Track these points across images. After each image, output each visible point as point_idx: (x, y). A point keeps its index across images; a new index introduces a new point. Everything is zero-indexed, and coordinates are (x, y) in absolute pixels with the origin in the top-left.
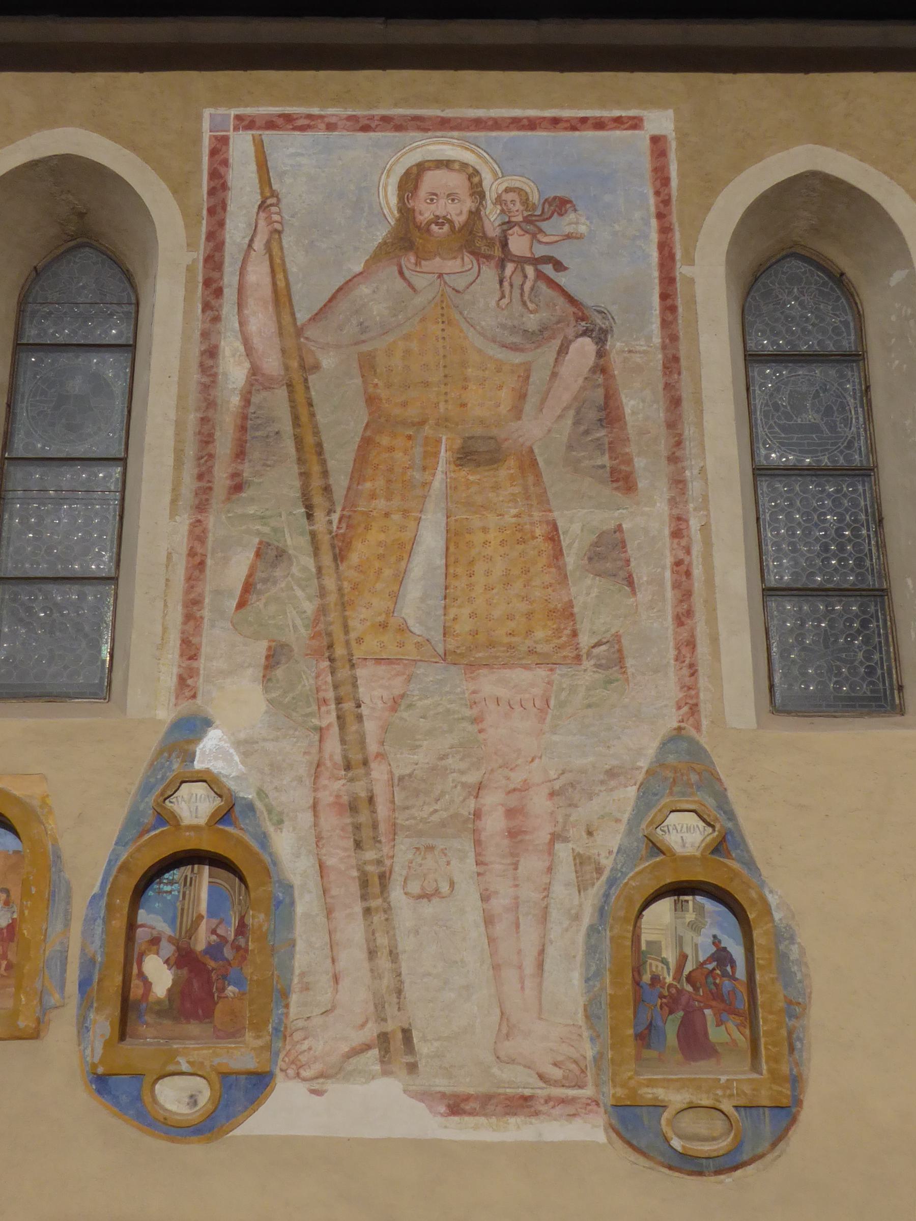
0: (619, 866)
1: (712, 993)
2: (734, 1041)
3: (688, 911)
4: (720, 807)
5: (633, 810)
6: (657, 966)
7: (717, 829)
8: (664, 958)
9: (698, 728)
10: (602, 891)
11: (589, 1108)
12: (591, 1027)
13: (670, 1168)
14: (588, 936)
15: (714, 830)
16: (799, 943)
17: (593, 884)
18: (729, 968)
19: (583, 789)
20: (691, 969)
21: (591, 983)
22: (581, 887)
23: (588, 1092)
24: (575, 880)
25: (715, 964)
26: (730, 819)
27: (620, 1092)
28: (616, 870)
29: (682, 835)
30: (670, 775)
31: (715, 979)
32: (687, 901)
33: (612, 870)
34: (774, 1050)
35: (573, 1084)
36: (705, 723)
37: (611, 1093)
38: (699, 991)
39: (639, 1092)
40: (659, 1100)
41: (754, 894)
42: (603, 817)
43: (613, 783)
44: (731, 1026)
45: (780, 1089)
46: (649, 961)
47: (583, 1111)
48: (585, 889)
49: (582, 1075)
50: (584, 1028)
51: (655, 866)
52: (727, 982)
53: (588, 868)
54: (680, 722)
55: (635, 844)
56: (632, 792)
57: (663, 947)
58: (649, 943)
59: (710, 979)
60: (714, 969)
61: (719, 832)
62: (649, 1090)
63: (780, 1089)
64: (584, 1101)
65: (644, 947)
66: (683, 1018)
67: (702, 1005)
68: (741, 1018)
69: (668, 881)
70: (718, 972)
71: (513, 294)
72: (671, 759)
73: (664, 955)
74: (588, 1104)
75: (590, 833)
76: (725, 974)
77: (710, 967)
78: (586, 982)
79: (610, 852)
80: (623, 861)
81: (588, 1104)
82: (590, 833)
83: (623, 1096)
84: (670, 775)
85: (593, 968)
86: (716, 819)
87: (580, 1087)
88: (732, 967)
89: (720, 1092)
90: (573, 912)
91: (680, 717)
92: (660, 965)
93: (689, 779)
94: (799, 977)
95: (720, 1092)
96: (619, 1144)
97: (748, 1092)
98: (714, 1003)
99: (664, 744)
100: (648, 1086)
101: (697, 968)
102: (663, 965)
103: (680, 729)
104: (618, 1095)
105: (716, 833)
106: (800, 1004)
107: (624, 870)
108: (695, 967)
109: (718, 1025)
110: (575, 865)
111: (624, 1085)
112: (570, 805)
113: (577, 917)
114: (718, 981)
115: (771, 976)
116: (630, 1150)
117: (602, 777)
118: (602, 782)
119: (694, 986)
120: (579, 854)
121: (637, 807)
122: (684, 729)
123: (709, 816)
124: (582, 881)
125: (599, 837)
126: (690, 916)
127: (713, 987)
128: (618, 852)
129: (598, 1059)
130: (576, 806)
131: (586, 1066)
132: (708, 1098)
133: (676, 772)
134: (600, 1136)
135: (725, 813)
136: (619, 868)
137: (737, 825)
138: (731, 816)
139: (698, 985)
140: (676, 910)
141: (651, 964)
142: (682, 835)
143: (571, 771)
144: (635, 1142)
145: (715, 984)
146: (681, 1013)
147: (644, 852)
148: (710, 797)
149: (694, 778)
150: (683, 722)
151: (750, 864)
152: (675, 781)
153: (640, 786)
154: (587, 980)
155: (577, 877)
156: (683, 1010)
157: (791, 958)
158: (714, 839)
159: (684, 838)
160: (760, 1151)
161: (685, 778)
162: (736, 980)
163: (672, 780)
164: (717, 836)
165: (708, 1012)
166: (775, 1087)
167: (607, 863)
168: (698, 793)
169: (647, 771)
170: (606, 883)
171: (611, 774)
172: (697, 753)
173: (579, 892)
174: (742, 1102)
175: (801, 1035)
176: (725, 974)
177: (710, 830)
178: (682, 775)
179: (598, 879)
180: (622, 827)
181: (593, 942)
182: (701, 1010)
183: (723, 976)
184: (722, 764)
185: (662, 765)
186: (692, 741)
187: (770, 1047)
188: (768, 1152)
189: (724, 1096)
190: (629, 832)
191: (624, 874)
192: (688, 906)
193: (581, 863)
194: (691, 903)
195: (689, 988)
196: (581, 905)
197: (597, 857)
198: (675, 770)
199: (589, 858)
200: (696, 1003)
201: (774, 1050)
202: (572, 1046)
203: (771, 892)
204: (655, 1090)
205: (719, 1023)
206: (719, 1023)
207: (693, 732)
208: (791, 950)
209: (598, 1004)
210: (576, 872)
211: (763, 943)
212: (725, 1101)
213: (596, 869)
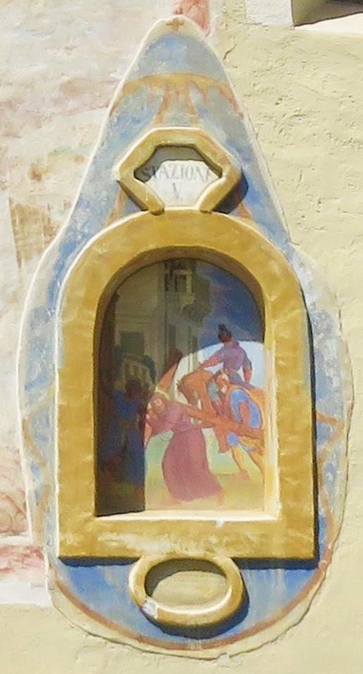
0: (79, 226)
1: (215, 407)
2: (243, 473)
3: (185, 290)
4: (231, 142)
5: (103, 144)
6: (136, 369)
7: (224, 174)
8: (147, 356)
9: (203, 23)
10: (52, 262)
11: (28, 560)
12: (34, 451)
13: (140, 639)
14: (32, 325)
15: (220, 176)
16: (339, 338)
17: (40, 251)
18: (241, 372)
19: (27, 111)
20: (186, 373)
21: (33, 390)
22: (22, 254)
23: (28, 538)
24: (14, 244)
25: (220, 366)
26: (247, 160)
27: (72, 539)
28: (75, 230)
29: (174, 181)
30: (159, 92)
31: (220, 386)
32: (184, 277)
33: (69, 229)
34: (295, 483)
35: (5, 528)
36: (214, 16)
37: (57, 544)
38: (196, 403)
39: (99, 539)
40: (127, 550)
41: (275, 268)
42: (56, 152)
43: (72, 104)
44: (241, 450)
45: (299, 535)
46: (125, 360)
47: (20, 565)
48: (28, 258)
49: (20, 517)
50: (22, 453)
51: (132, 226)
52: (236, 390)
53: (34, 227)
54: (177, 13)
55: (104, 193)
56: (102, 118)
57: (147, 339)
58: (125, 336)
59: (214, 387)
60: (219, 373)
61: (229, 177)
62: (114, 536)
63: (299, 535)
64: (21, 551)
65: (117, 341)
66: (171, 440)
67: (200, 422)
68: (255, 441)
69: (152, 246)
70: (225, 376)
71: (345, 451)
72: (162, 70)
73: (147, 353)
74: (27, 556)
75: (36, 176)
76: (234, 381)
77: (213, 370)
78: (26, 388)
79: (67, 205)
80: (85, 218)
81: (27, 556)
82: (36, 176)
83: (75, 544)
84: (159, 92)
85: (39, 369)
86: (225, 160)
87: (16, 533)
88: (245, 371)
89: (214, 540)
90: (10, 290)
91: (177, 6)
92: (141, 367)
93: (188, 99)
94: (335, 383)
95: (214, 540)
96: (69, 608)
97: (254, 539)
98: (217, 421)
99: (151, 47)
100: (112, 531)
101: (195, 372)
102: (145, 367)
103: (175, 24)
104: (69, 543)
105: (223, 179)
106: (334, 420)
107: (86, 231)
108: (191, 370)
109: (222, 451)
110: (14, 222)
111: (78, 530)
112: (7, 135)
113: (16, 298)
114: (224, 390)
115: (296, 382)
116: (84, 615)
117: (56, 94)
118: (56, 102)
119: (189, 397)
120: (19, 206)
121: (107, 139)
122: (182, 24)
123: (214, 154)
124: (24, 246)
125: (50, 183)
126: (187, 299)
127: (217, 398)
128: (78, 205)
129: (42, 496)
130: (16, 136)
131: (25, 504)
132: (197, 547)
133: (168, 89)
134: (45, 599)
135: (239, 150)
136: (79, 229)
137: (256, 168)
138: (247, 154)
139: (196, 394)
140: (167, 289)
141: (127, 366)
142: (174, 181)
143: (10, 84)
144: (91, 606)
145: (220, 394)
146: (170, 434)
147: (116, 205)
148: (217, 127)
149: (195, 97)
150: (181, 13)
151: (275, 227)
152: (166, 102)
153: (114, 108)
154: (28, 386)
155: (16, 241)
156: (172, 430)
157: (326, 359)
158: (220, 188)
159: (178, 187)
160: (268, 617)
161: (182, 97)
162: (251, 388)
163: (162, 99)
164: (226, 184)
165: (208, 433)
166: (291, 532)
167: (63, 222)
168: (201, 120)
169: (125, 86)
170: (60, 250)
171: (71, 89)
172: (201, 58)
173: (19, 261)
174: (244, 553)
175: (334, 464)
176: (234, 381)
177: (214, 175)
178: (178, 93)
179: (48, 243)
180: (86, 168)
181: (38, 333)
182: (198, 430)
183: (231, 383)
184: (238, 73)
185: (149, 79)
186: (192, 43)
187: (288, 479)
188: (279, 619)
189: (219, 544)
190: (95, 176)
191: (86, 237)
192: (185, 284)
193: (22, 221)
194: (189, 281)
195: (182, 399)
196: (21, 281)
197: (46, 212)
198: (167, 85)
199: (35, 212)
200: (192, 420)
201: (295, 483)
202: (5, 477)
203: (302, 265)
204: (122, 537)
205: (224, 448)
206: (224, 448)
207: (197, 30)
208: (326, 347)
209: (44, 420)
210: (15, 233)
211: (287, 337)
212: (220, 551)
213: (45, 228)
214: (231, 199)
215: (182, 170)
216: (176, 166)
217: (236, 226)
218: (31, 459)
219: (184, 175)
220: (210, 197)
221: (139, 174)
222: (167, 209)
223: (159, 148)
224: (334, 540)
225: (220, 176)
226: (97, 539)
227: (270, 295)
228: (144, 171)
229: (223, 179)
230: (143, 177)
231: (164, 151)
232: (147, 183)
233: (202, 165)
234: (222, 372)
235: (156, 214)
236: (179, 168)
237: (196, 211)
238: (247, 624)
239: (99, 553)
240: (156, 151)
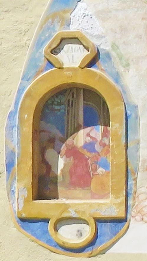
7: (90, 50)
61: (92, 51)
214: (93, 62)
215: (72, 48)
216: (69, 47)
217: (95, 74)
218: (46, 192)
219: (73, 51)
220: (84, 60)
221: (53, 52)
222: (64, 66)
223: (62, 40)
224: (66, 121)
225: (89, 51)
226: (119, 124)
227: (123, 109)
228: (55, 51)
229: (90, 52)
230: (55, 54)
231: (64, 41)
232: (57, 56)
233: (81, 46)
234: (101, 69)
235: (59, 68)
236: (71, 48)
237: (77, 67)
238: (99, 247)
239: (50, 251)
240: (61, 41)
